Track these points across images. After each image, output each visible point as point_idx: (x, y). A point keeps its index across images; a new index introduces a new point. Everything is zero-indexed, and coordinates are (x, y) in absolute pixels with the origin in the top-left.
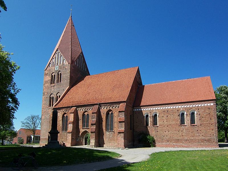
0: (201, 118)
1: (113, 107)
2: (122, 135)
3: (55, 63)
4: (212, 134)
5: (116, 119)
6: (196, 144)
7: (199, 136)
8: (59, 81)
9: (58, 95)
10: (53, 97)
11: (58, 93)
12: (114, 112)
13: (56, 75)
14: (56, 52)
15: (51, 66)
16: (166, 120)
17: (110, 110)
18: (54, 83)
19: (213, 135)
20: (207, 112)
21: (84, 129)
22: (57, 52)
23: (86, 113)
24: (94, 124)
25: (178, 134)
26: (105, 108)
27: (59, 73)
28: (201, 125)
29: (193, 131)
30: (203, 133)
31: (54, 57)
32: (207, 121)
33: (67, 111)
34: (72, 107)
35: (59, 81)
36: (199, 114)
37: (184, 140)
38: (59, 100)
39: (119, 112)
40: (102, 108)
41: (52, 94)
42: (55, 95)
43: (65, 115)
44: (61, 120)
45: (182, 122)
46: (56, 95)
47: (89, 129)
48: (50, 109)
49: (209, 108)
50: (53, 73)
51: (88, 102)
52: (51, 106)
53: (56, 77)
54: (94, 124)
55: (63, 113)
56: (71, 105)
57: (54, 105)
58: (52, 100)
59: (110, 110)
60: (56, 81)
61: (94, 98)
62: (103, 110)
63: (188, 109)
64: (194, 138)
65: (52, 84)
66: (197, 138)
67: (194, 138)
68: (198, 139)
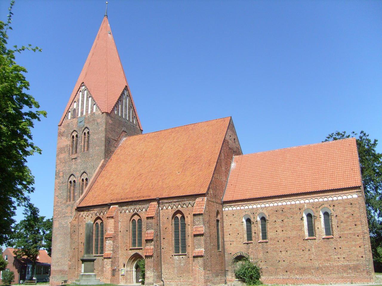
0: (339, 223)
4: (360, 256)
6: (335, 276)
16: (281, 229)
18: (76, 152)
19: (362, 257)
20: (349, 210)
25: (302, 256)
28: (340, 237)
29: (328, 251)
32: (350, 229)
33: (102, 214)
36: (336, 216)
37: (313, 269)
47: (142, 249)
48: (69, 208)
52: (70, 201)
64: (331, 263)
67: (331, 263)
68: (338, 266)
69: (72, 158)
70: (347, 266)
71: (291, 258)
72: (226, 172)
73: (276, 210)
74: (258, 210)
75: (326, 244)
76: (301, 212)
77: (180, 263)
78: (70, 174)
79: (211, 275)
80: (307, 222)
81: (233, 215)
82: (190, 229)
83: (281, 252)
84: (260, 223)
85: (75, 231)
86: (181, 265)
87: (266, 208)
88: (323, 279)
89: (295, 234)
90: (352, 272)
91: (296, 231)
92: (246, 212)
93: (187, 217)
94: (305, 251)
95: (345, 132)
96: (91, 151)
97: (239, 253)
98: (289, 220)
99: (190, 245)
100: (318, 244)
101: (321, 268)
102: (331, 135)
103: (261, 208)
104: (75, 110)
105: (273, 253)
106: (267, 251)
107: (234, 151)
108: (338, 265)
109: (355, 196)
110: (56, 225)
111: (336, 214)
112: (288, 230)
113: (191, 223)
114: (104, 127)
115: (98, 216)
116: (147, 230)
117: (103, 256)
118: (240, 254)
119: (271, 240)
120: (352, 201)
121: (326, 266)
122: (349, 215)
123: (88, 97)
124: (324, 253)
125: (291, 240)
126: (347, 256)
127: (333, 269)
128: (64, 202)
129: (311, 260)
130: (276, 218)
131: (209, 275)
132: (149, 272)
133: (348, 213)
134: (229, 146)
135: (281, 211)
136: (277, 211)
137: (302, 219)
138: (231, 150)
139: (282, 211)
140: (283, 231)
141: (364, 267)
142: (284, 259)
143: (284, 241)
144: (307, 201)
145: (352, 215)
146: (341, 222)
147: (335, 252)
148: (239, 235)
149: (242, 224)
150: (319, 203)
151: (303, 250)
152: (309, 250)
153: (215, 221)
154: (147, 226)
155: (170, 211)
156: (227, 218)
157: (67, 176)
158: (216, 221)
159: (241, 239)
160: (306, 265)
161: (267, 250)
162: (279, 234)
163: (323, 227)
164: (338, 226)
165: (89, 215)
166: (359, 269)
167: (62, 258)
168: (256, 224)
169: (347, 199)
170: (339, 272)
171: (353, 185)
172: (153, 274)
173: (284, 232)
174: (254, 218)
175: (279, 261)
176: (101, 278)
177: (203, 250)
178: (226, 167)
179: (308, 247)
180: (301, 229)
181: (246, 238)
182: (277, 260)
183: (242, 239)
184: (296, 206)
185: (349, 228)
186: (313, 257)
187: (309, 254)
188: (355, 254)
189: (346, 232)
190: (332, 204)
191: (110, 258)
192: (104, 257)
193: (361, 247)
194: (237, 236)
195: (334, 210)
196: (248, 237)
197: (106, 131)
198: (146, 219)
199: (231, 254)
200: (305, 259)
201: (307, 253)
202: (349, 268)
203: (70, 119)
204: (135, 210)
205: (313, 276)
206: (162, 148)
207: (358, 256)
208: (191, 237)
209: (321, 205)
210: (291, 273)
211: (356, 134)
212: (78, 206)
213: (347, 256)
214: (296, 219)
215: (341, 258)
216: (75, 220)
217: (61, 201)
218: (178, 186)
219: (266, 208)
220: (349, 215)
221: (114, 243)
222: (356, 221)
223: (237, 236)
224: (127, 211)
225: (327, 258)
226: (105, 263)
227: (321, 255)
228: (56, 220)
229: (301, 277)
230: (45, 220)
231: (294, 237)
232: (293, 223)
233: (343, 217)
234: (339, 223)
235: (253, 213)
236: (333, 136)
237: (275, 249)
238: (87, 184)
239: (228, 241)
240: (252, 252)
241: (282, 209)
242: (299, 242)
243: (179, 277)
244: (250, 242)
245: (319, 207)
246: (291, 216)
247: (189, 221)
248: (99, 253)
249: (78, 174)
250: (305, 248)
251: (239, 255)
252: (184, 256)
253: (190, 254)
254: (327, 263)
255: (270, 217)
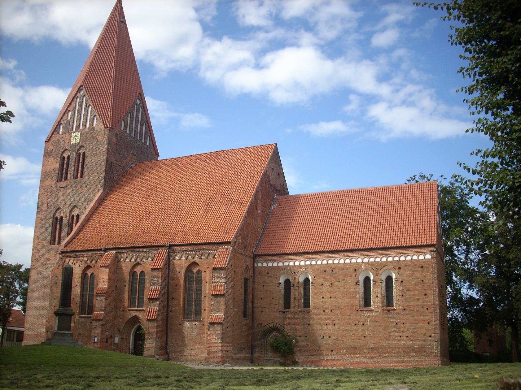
0: (405, 291)
1: (202, 255)
2: (218, 329)
3: (71, 123)
4: (428, 334)
5: (207, 289)
6: (394, 359)
7: (399, 338)
8: (79, 174)
9: (75, 213)
10: (62, 217)
11: (75, 206)
12: (203, 270)
13: (73, 157)
14: (76, 95)
15: (61, 133)
16: (328, 295)
17: (195, 264)
18: (66, 179)
19: (430, 336)
20: (418, 275)
21: (132, 310)
22: (79, 95)
23: (138, 270)
24: (156, 299)
25: (354, 332)
26: (183, 258)
27: (81, 152)
28: (405, 309)
29: (388, 326)
30: (408, 332)
31: (71, 109)
32: (418, 299)
33: (94, 262)
34: (106, 250)
35: (79, 174)
36: (402, 282)
37: (366, 349)
38: (75, 229)
39: (215, 269)
40: (177, 258)
41: (59, 208)
42: (66, 212)
43: (89, 272)
44: (79, 284)
45: (367, 302)
46: (68, 215)
47: (143, 310)
48: (53, 253)
49: (422, 267)
50: (66, 150)
51: (143, 240)
52: (54, 244)
53: (72, 163)
54: (156, 299)
55: (83, 266)
56: (103, 247)
57: (63, 243)
58: (58, 226)
59: (195, 264)
60: (71, 171)
61: (161, 227)
62: (179, 261)
63: (377, 268)
64: (390, 342)
65: (61, 180)
66: (395, 344)
67: (390, 342)
68: (399, 347)
69: (61, 187)
70: (410, 347)
71: (339, 333)
72: (262, 216)
73: (325, 269)
74: (301, 268)
75: (385, 317)
76: (356, 274)
77: (192, 331)
78: (57, 208)
79: (231, 349)
80: (363, 287)
81: (268, 273)
82: (207, 288)
83: (327, 325)
84: (303, 286)
85: (57, 283)
86: (193, 334)
87: (311, 267)
88: (378, 362)
89: (347, 303)
90: (416, 355)
91: (348, 298)
92: (285, 270)
93: (205, 272)
94: (358, 326)
95: (432, 175)
96: (86, 178)
97: (272, 324)
98: (339, 283)
99: (206, 309)
100: (375, 317)
101: (377, 349)
102: (413, 178)
103: (306, 266)
104: (68, 122)
105: (317, 326)
106: (308, 323)
107: (276, 190)
108: (398, 346)
109: (428, 257)
110: (33, 275)
111: (402, 279)
112: (338, 297)
113: (209, 279)
114: (106, 147)
115: (88, 264)
116: (151, 285)
117: (91, 317)
118: (274, 325)
119: (315, 308)
120: (423, 263)
121: (384, 345)
122: (418, 281)
123: (88, 105)
124: (382, 329)
125: (341, 311)
126: (411, 334)
127: (392, 350)
128: (46, 245)
129: (365, 337)
130: (324, 280)
131: (229, 349)
132: (150, 341)
133: (417, 278)
134: (271, 182)
135: (331, 272)
136: (325, 271)
137: (358, 283)
138: (272, 188)
139: (332, 271)
140: (331, 297)
141: (431, 350)
142: (330, 335)
143: (332, 311)
144: (366, 260)
145: (423, 281)
146: (407, 290)
147: (397, 329)
148: (273, 300)
149: (278, 286)
150: (381, 264)
151: (355, 324)
152: (363, 324)
153: (242, 279)
154: (151, 280)
155: (183, 263)
156: (260, 277)
157: (53, 210)
158: (243, 280)
159: (276, 305)
160: (359, 343)
161: (309, 321)
162: (325, 302)
163: (384, 296)
164: (402, 295)
165: (77, 262)
166: (425, 351)
167: (39, 318)
168: (297, 286)
169: (418, 260)
170: (399, 355)
171: (427, 242)
172: (154, 344)
173: (333, 299)
174: (295, 279)
175: (323, 337)
176: (87, 346)
177: (222, 315)
178: (264, 210)
179: (362, 320)
180: (355, 297)
181: (283, 305)
182: (320, 336)
183: (277, 306)
184: (351, 265)
185: (417, 298)
186: (367, 333)
187: (363, 330)
188: (422, 332)
189: (412, 303)
190: (397, 265)
191: (100, 320)
192: (92, 318)
193: (431, 324)
194: (271, 301)
195: (400, 273)
196: (285, 304)
197: (108, 153)
198: (150, 272)
199: (261, 324)
200: (358, 335)
201: (361, 328)
202: (413, 350)
203: (61, 134)
204: (138, 259)
205: (366, 357)
206: (180, 180)
207: (425, 335)
208: (209, 298)
209: (384, 267)
210: (337, 353)
211: (445, 179)
212: (63, 250)
213: (411, 334)
214: (350, 283)
215: (403, 336)
216: (58, 269)
217: (43, 243)
218: (197, 230)
219: (311, 267)
220: (418, 281)
221: (107, 301)
222: (427, 290)
223: (271, 301)
224: (127, 260)
225: (385, 336)
226: (94, 327)
227: (378, 332)
228: (34, 268)
229: (350, 359)
230: (22, 270)
231: (345, 307)
232: (345, 288)
233: (410, 283)
234: (405, 291)
235: (294, 273)
236: (415, 178)
237: (319, 321)
238: (77, 221)
239: (259, 308)
240: (289, 323)
241: (333, 270)
242: (352, 313)
243: (189, 350)
244: (287, 310)
245: (381, 269)
246: (344, 278)
247: (208, 278)
248: (86, 314)
249: (67, 209)
250: (359, 322)
251: (272, 326)
252: (197, 323)
253: (206, 320)
254: (385, 342)
255: (315, 278)
